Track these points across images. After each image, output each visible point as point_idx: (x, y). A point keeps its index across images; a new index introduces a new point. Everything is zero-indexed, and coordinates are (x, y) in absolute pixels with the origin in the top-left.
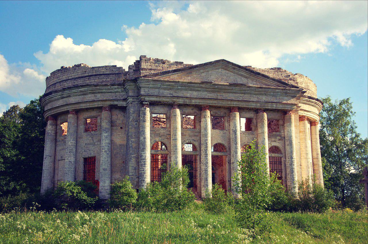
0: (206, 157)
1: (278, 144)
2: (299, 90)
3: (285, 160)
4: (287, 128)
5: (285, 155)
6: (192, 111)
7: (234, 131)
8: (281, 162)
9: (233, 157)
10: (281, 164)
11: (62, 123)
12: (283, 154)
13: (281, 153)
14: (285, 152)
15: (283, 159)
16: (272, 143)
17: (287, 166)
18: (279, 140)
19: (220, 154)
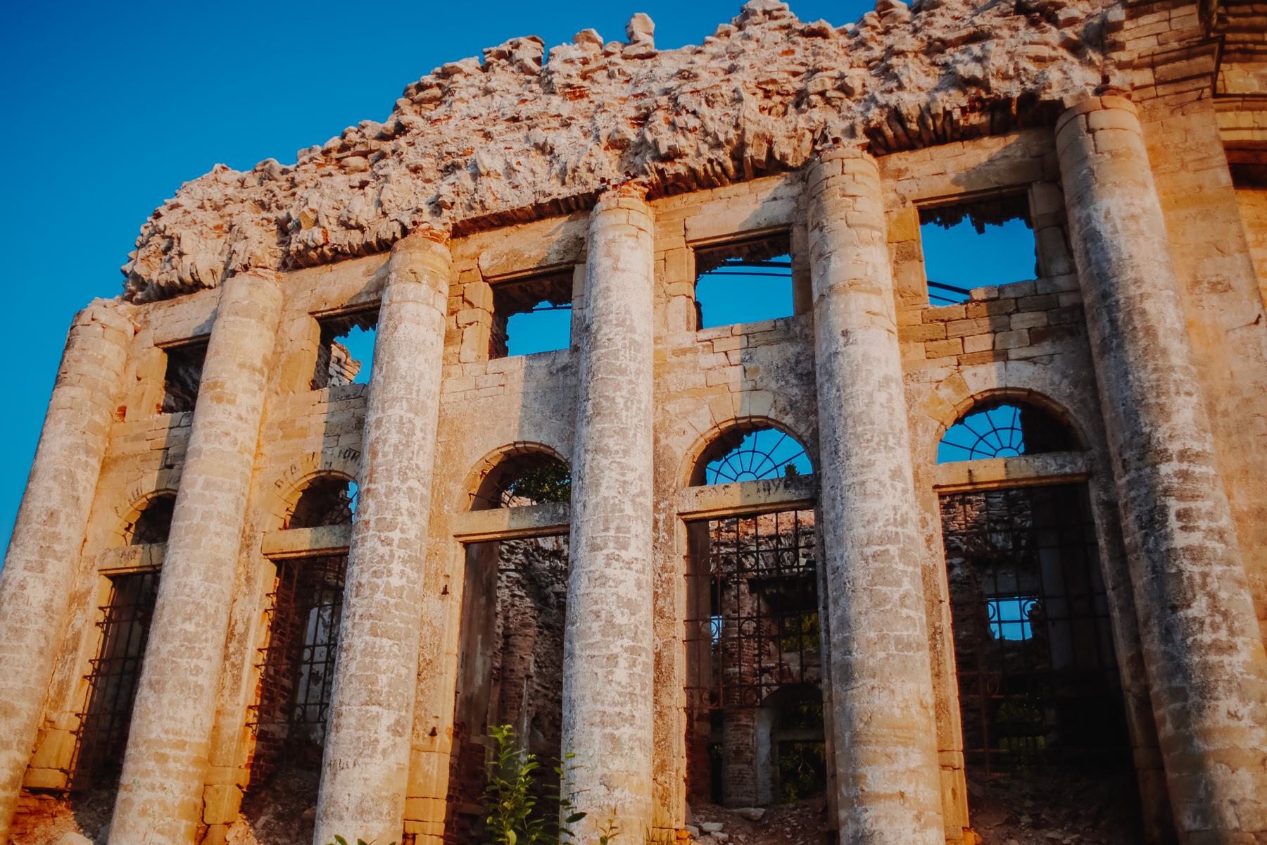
12: (1096, 451)
18: (1036, 336)
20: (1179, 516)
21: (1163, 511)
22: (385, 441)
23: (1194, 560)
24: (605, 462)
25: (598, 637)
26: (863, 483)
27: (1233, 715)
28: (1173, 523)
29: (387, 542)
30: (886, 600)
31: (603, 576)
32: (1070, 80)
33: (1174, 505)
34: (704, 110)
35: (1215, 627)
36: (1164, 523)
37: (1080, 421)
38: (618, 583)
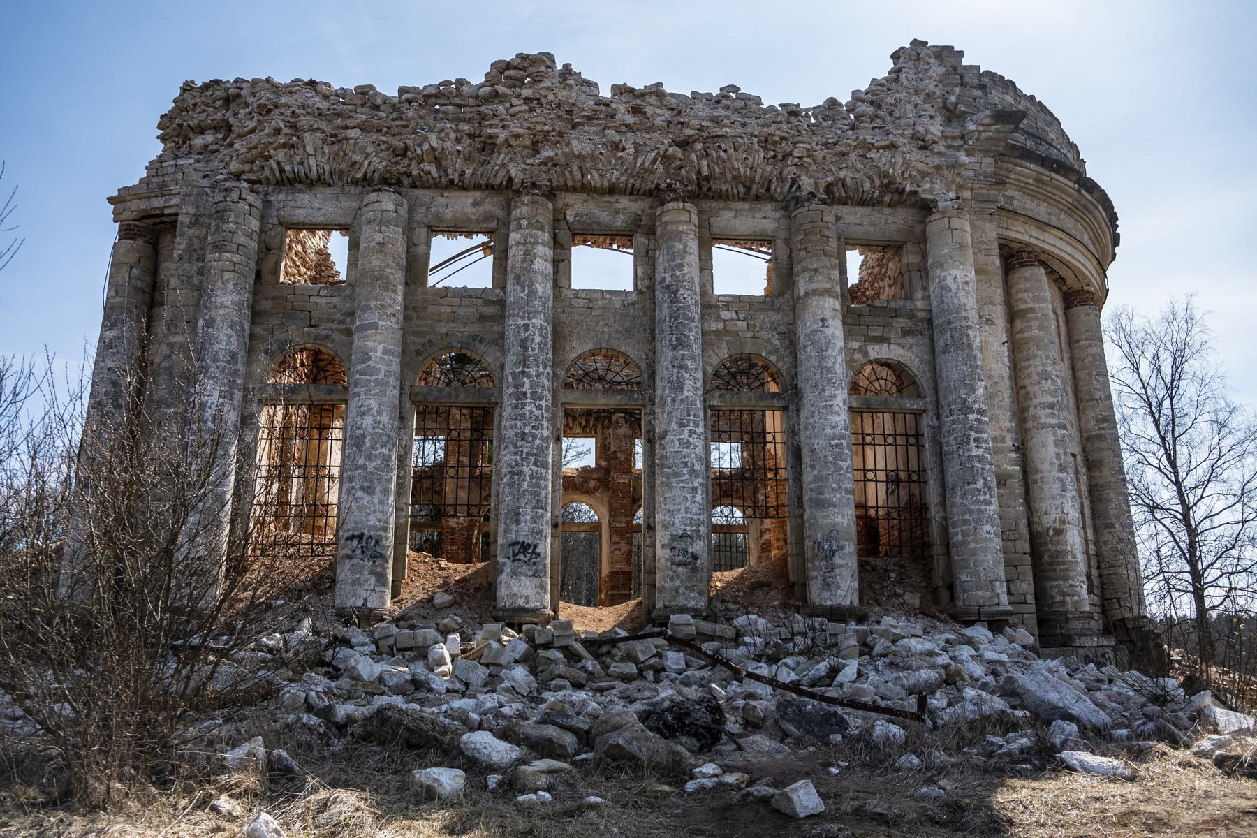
0: (516, 406)
1: (900, 350)
2: (1104, 253)
3: (936, 422)
4: (938, 272)
5: (937, 401)
6: (474, 210)
7: (668, 287)
8: (918, 435)
9: (663, 406)
10: (919, 446)
11: (921, 598)
12: (928, 399)
13: (919, 396)
14: (936, 389)
15: (927, 421)
16: (869, 348)
17: (945, 449)
18: (906, 333)
19: (603, 401)
20: (975, 440)
21: (968, 437)
22: (532, 340)
23: (980, 462)
24: (686, 375)
25: (686, 477)
26: (831, 406)
27: (988, 532)
28: (973, 444)
29: (539, 407)
30: (841, 469)
31: (688, 442)
32: (938, 191)
33: (974, 435)
34: (731, 151)
35: (985, 494)
36: (968, 444)
37: (925, 383)
38: (696, 446)
